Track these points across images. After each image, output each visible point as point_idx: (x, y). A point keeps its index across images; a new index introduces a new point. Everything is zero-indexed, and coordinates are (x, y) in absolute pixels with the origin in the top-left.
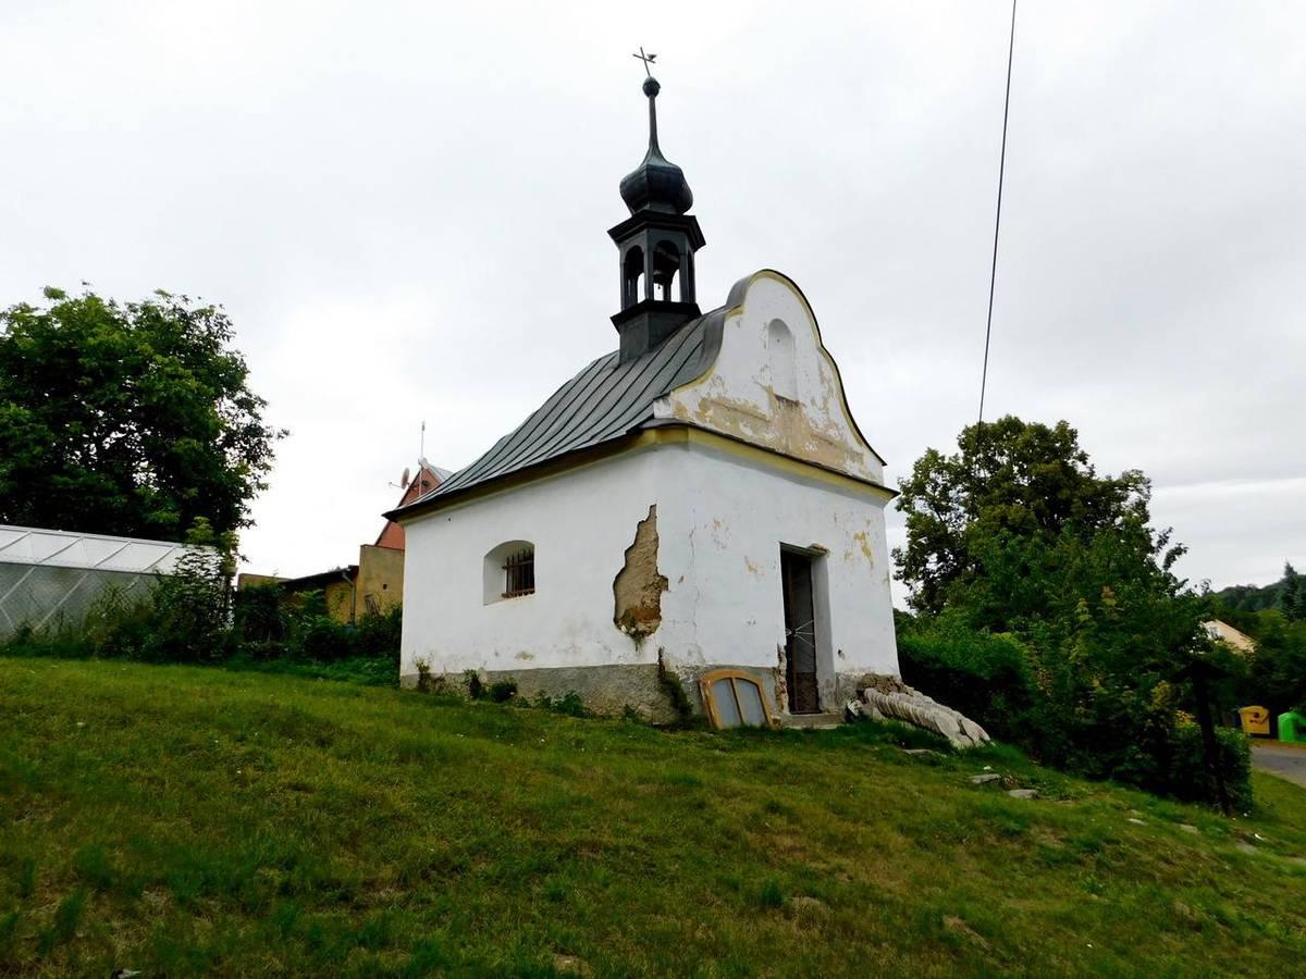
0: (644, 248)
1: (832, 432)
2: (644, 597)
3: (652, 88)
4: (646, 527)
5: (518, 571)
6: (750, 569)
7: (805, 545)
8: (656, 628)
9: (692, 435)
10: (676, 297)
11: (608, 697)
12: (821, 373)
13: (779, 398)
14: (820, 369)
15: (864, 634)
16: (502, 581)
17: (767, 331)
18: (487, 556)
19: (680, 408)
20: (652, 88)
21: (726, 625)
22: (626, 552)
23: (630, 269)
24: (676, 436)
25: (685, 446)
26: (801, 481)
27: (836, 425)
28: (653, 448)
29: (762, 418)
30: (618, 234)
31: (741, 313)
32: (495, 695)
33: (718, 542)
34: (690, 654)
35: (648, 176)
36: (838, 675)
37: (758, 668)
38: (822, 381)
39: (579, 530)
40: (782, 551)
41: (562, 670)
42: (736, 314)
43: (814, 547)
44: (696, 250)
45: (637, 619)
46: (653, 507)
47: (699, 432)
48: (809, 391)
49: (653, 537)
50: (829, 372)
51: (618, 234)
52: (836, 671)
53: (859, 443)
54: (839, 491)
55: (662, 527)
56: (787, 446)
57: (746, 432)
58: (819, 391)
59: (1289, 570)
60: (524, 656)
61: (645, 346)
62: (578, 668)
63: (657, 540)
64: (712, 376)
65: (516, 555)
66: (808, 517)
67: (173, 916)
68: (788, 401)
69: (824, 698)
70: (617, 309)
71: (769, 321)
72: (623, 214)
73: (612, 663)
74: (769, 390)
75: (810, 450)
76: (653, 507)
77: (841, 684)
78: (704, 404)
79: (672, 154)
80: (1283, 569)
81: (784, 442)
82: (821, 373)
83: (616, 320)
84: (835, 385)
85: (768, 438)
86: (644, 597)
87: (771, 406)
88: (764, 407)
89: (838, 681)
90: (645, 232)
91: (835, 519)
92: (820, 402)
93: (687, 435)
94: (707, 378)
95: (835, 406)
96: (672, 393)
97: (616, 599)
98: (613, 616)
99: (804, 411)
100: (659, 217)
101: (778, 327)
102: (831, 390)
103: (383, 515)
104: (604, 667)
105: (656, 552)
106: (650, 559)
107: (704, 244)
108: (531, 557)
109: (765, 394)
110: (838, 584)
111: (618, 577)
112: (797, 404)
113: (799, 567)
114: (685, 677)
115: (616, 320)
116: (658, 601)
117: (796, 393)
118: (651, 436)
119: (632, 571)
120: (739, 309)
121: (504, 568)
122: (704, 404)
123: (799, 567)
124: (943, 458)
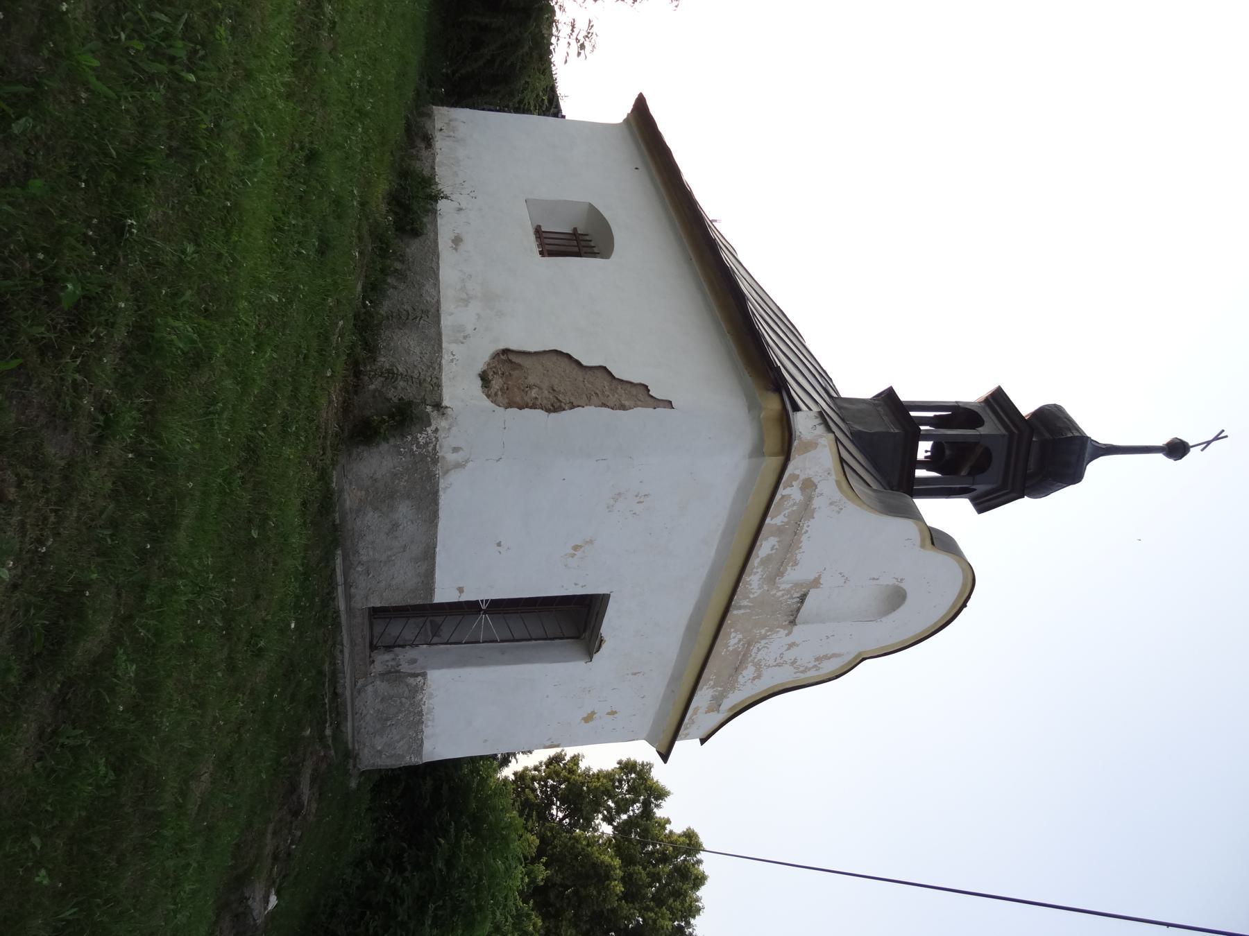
0: (982, 430)
1: (749, 671)
2: (540, 388)
3: (1177, 449)
4: (640, 394)
5: (577, 240)
6: (576, 548)
7: (606, 629)
8: (494, 402)
9: (774, 462)
10: (920, 473)
11: (402, 348)
12: (827, 657)
13: (803, 598)
14: (834, 655)
15: (475, 712)
16: (558, 225)
17: (891, 582)
18: (591, 206)
19: (810, 446)
20: (1177, 449)
21: (498, 514)
22: (605, 368)
23: (959, 415)
24: (773, 439)
25: (758, 451)
26: (692, 628)
27: (759, 677)
28: (753, 406)
29: (780, 573)
30: (998, 400)
31: (923, 546)
32: (412, 204)
33: (616, 500)
34: (456, 450)
35: (1075, 437)
36: (424, 675)
37: (434, 558)
39: (627, 312)
40: (598, 595)
41: (436, 284)
42: (923, 540)
44: (973, 500)
45: (510, 377)
46: (669, 404)
47: (778, 471)
48: (808, 640)
49: (627, 403)
50: (829, 667)
51: (998, 400)
53: (731, 709)
54: (675, 679)
55: (641, 414)
56: (740, 608)
57: (766, 547)
58: (805, 655)
60: (457, 241)
61: (858, 428)
62: (438, 302)
64: (845, 500)
65: (592, 244)
66: (646, 629)
68: (798, 610)
70: (904, 396)
72: (1026, 408)
73: (444, 345)
74: (816, 583)
75: (732, 639)
76: (669, 404)
77: (411, 681)
78: (809, 486)
79: (1096, 469)
81: (745, 603)
82: (827, 657)
83: (889, 395)
84: (812, 674)
85: (754, 581)
86: (540, 388)
87: (797, 585)
88: (794, 575)
89: (415, 675)
90: (1004, 432)
92: (789, 656)
93: (775, 455)
94: (847, 497)
95: (785, 675)
96: (831, 436)
97: (536, 353)
98: (512, 348)
99: (783, 632)
100: (1021, 452)
101: (896, 598)
102: (807, 669)
103: (641, 106)
104: (440, 334)
105: (604, 405)
106: (594, 398)
107: (980, 511)
108: (593, 254)
109: (812, 577)
110: (550, 678)
111: (569, 356)
112: (793, 623)
113: (573, 621)
114: (422, 441)
115: (889, 395)
116: (534, 407)
117: (806, 622)
118: (772, 404)
119: (579, 374)
120: (928, 541)
121: (575, 229)
122: (809, 486)
123: (573, 621)
124: (658, 806)
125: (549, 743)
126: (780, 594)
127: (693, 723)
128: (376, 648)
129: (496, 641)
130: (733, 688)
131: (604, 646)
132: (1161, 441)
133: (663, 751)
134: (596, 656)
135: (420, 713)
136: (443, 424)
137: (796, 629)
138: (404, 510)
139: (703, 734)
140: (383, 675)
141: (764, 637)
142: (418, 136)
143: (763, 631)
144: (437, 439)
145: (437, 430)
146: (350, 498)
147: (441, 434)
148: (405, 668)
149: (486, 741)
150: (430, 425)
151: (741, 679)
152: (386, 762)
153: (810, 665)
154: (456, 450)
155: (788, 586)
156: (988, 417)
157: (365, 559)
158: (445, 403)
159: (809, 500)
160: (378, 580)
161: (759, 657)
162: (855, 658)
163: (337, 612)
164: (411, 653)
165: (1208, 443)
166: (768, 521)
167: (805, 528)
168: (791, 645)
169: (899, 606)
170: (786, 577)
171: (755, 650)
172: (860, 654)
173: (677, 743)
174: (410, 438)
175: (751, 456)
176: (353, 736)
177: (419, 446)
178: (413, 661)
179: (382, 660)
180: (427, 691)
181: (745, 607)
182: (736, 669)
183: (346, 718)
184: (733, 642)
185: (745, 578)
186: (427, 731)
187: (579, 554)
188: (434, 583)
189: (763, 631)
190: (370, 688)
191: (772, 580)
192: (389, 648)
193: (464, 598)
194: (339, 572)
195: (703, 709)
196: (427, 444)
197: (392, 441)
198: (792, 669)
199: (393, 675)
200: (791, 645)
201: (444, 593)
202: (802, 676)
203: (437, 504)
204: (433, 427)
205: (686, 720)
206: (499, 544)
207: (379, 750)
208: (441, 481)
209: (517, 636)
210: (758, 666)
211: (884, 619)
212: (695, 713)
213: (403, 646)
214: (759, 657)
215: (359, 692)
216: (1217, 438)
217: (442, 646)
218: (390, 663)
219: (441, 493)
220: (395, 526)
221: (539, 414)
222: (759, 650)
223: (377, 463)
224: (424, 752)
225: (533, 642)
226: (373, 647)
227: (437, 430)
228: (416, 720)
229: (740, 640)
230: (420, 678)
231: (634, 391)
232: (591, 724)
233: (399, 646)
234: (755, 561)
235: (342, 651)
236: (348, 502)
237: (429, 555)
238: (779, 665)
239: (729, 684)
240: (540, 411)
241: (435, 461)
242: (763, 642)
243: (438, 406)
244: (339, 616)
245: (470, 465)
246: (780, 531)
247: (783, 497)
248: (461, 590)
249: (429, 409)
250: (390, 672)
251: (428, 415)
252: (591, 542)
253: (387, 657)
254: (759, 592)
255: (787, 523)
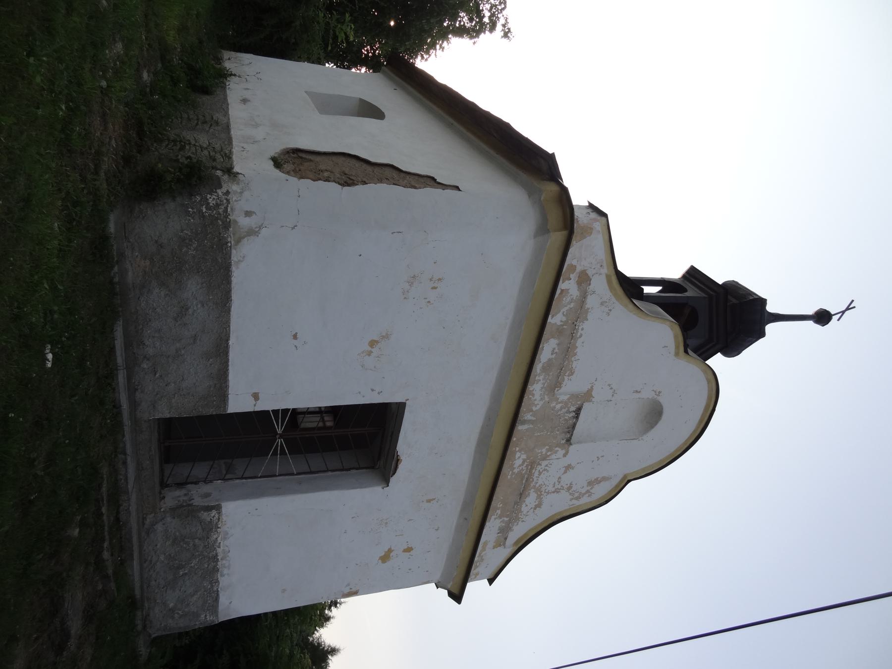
1: (531, 499)
3: (822, 317)
6: (373, 343)
7: (402, 447)
9: (558, 237)
12: (598, 481)
14: (605, 479)
18: (361, 99)
20: (822, 317)
25: (543, 230)
27: (539, 506)
28: (531, 193)
31: (677, 354)
33: (411, 284)
34: (248, 214)
36: (218, 508)
38: (591, 483)
42: (677, 347)
43: (398, 461)
48: (581, 461)
50: (600, 491)
52: (223, 504)
53: (516, 543)
54: (467, 505)
56: (524, 422)
59: (333, 651)
63: (415, 188)
64: (614, 300)
67: (112, 199)
69: (184, 491)
71: (661, 399)
74: (588, 396)
75: (518, 460)
77: (204, 515)
78: (584, 279)
80: (333, 645)
82: (598, 481)
84: (585, 501)
85: (536, 388)
87: (574, 396)
88: (571, 386)
89: (209, 509)
91: (429, 501)
92: (566, 479)
94: (615, 295)
95: (554, 504)
99: (561, 452)
101: (654, 414)
109: (585, 389)
114: (212, 202)
117: (579, 442)
125: (347, 590)
126: (558, 406)
127: (482, 560)
128: (167, 486)
129: (292, 474)
130: (517, 519)
131: (400, 466)
132: (811, 312)
133: (456, 591)
134: (393, 480)
135: (215, 559)
136: (235, 188)
137: (572, 448)
138: (193, 287)
139: (490, 574)
140: (174, 511)
141: (545, 458)
142: (207, 82)
143: (544, 451)
144: (228, 201)
145: (228, 193)
146: (133, 268)
147: (233, 198)
148: (198, 501)
149: (284, 591)
150: (220, 187)
151: (524, 509)
152: (178, 624)
153: (583, 491)
154: (248, 214)
155: (565, 398)
156: (687, 285)
157: (151, 351)
158: (237, 169)
159: (584, 296)
160: (166, 392)
161: (540, 482)
162: (621, 481)
163: (117, 406)
164: (205, 488)
165: (843, 312)
166: (549, 320)
167: (580, 332)
168: (568, 467)
169: (656, 423)
170: (563, 389)
171: (536, 474)
172: (625, 476)
173: (469, 585)
174: (198, 198)
175: (535, 237)
176: (142, 587)
177: (208, 208)
178: (207, 495)
179: (172, 497)
180: (223, 528)
181: (529, 422)
182: (521, 494)
183: (132, 555)
184: (518, 462)
185: (530, 387)
186: (223, 581)
187: (375, 350)
188: (227, 387)
189: (544, 451)
190: (159, 527)
191: (554, 387)
192: (181, 485)
193: (261, 406)
194: (119, 344)
195: (491, 545)
196: (217, 205)
197: (179, 199)
198: (564, 494)
199: (187, 511)
200: (568, 467)
201: (239, 402)
202: (576, 503)
203: (229, 282)
204: (224, 190)
205: (476, 559)
206: (295, 337)
207: (169, 611)
208: (234, 252)
209: (313, 470)
210: (539, 491)
211: (645, 437)
212: (484, 549)
213: (196, 483)
214: (540, 482)
215: (148, 533)
216: (848, 309)
217: (238, 481)
218: (181, 499)
219: (233, 268)
220: (184, 310)
221: (333, 187)
222: (540, 473)
223: (164, 224)
224: (221, 608)
225: (330, 473)
226: (163, 485)
227: (228, 193)
228: (209, 568)
229: (524, 461)
230: (214, 513)
231: (422, 180)
232: (388, 564)
233: (192, 483)
234: (538, 367)
235: (125, 463)
236: (130, 274)
237: (220, 351)
238: (557, 491)
239: (513, 515)
240: (334, 184)
241: (227, 225)
242: (544, 463)
243: (229, 171)
244: (119, 414)
245: (264, 231)
246: (559, 332)
247: (562, 291)
248: (256, 396)
249: (219, 173)
250: (182, 506)
251: (218, 178)
252: (386, 337)
253: (178, 493)
254: (541, 403)
255: (566, 323)
